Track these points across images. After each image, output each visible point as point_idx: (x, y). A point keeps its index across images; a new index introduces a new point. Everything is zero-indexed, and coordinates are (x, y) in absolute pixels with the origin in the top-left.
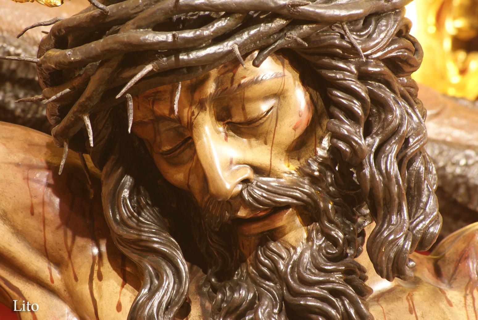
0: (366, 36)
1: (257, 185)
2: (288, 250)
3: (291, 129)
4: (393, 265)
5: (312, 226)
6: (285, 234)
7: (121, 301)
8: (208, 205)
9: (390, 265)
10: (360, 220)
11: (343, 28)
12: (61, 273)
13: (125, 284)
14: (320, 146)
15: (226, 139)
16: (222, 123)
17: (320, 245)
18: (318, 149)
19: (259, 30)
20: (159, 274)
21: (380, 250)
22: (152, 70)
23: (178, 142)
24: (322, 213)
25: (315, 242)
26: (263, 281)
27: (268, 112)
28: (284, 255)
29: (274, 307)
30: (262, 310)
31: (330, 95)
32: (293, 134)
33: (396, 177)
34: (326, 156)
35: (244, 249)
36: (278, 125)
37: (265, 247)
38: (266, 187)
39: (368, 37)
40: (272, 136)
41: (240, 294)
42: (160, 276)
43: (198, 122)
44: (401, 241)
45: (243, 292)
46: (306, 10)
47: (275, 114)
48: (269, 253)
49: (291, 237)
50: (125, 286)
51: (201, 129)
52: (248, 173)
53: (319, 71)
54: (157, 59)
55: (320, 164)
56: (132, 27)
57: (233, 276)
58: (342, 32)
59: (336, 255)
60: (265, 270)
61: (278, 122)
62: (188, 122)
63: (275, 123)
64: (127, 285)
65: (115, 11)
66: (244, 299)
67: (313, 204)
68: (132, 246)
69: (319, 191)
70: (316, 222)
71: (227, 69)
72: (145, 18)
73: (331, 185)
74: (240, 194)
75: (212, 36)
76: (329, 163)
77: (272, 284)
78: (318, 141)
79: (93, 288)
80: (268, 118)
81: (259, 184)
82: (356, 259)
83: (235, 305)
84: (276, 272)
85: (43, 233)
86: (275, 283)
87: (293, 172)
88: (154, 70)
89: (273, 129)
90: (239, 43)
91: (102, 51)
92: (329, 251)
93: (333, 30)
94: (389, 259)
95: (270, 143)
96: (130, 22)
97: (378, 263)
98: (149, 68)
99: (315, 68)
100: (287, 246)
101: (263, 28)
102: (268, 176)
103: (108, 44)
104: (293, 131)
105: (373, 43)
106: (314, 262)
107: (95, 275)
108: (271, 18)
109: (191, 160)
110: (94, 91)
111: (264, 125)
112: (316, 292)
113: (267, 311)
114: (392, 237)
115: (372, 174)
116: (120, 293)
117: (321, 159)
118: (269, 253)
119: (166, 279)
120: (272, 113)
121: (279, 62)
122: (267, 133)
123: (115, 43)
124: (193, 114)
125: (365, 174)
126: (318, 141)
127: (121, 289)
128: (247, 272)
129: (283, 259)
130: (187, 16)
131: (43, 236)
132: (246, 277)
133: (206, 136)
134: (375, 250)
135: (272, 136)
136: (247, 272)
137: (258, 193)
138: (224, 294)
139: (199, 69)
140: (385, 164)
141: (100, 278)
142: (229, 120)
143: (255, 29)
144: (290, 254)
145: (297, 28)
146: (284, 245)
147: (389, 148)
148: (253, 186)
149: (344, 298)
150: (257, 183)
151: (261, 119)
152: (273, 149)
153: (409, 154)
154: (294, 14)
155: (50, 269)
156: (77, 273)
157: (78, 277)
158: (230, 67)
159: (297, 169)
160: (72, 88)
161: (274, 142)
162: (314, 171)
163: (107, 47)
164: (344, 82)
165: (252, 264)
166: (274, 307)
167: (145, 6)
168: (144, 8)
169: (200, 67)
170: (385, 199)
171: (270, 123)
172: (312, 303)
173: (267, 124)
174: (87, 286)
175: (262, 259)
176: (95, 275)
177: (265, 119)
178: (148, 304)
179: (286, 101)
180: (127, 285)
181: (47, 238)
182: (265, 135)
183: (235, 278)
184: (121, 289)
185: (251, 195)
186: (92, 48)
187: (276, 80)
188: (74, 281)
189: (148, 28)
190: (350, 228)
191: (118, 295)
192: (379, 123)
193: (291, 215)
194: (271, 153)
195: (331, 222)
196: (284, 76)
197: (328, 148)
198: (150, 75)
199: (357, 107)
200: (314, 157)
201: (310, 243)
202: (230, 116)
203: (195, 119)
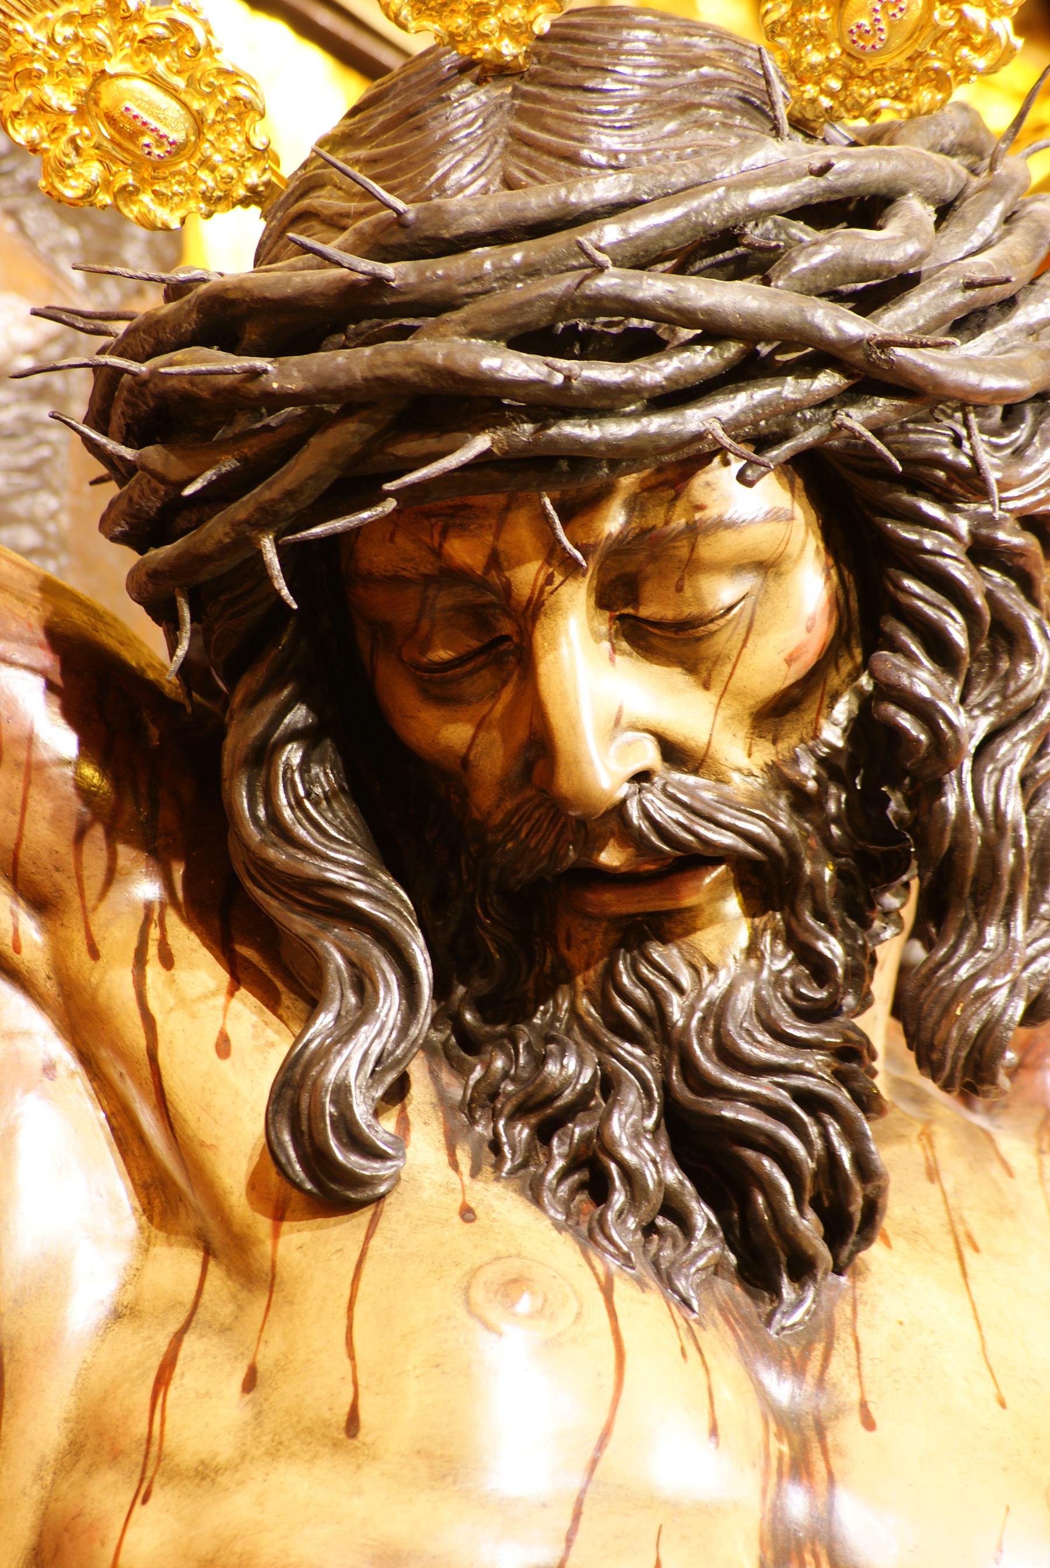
0: (1009, 451)
1: (664, 791)
2: (696, 970)
3: (779, 660)
4: (969, 1054)
5: (765, 918)
6: (694, 930)
7: (230, 1032)
8: (513, 822)
9: (963, 1054)
10: (877, 924)
11: (966, 424)
12: (44, 928)
13: (237, 989)
14: (828, 717)
15: (612, 660)
16: (608, 614)
17: (781, 972)
18: (823, 722)
19: (780, 393)
20: (367, 981)
21: (947, 1009)
22: (488, 452)
23: (475, 644)
24: (803, 889)
25: (767, 962)
26: (616, 1040)
27: (730, 609)
28: (685, 979)
29: (646, 1113)
30: (623, 1117)
31: (891, 588)
32: (783, 673)
33: (1016, 829)
34: (840, 744)
35: (569, 947)
36: (749, 645)
37: (635, 952)
38: (685, 798)
39: (1013, 453)
40: (728, 669)
41: (562, 1066)
42: (369, 987)
43: (557, 602)
44: (999, 998)
45: (571, 1063)
46: (909, 360)
47: (747, 614)
48: (645, 970)
49: (706, 940)
50: (237, 993)
51: (561, 622)
52: (649, 756)
53: (878, 519)
54: (506, 424)
55: (821, 761)
56: (462, 329)
57: (534, 1015)
58: (964, 432)
59: (819, 1005)
60: (628, 1011)
61: (752, 637)
62: (530, 600)
63: (742, 637)
64: (243, 992)
65: (412, 279)
66: (567, 1083)
67: (786, 863)
68: (293, 893)
69: (806, 830)
70: (775, 910)
71: (661, 478)
72: (497, 313)
73: (837, 820)
74: (620, 808)
75: (662, 387)
76: (842, 763)
77: (639, 1052)
78: (827, 701)
79: (144, 984)
80: (730, 621)
81: (670, 790)
82: (855, 1021)
83: (547, 1091)
84: (657, 1023)
85: (18, 818)
86: (648, 1052)
87: (757, 772)
88: (495, 450)
89: (735, 653)
90: (724, 418)
91: (365, 380)
92: (803, 990)
93: (938, 421)
94: (964, 1036)
95: (717, 687)
96: (455, 316)
97: (936, 1042)
98: (482, 443)
99: (867, 512)
100: (695, 961)
101: (791, 388)
102: (695, 772)
103: (386, 364)
104: (784, 666)
105: (1028, 470)
106: (764, 1015)
107: (153, 951)
108: (808, 367)
109: (493, 696)
110: (310, 477)
111: (716, 639)
112: (764, 1091)
113: (631, 1121)
114: (981, 984)
115: (962, 811)
116: (225, 1009)
117: (826, 750)
118: (645, 970)
119: (386, 994)
120: (742, 609)
121: (785, 480)
122: (718, 660)
123: (408, 364)
124: (549, 580)
125: (944, 809)
126: (827, 701)
127: (228, 1001)
128: (573, 1010)
129: (680, 990)
130: (593, 324)
131: (16, 825)
132: (567, 1024)
133: (570, 644)
134: (931, 1010)
135: (728, 669)
136: (573, 1010)
137: (667, 814)
138: (513, 1059)
139: (601, 468)
140: (993, 789)
141: (167, 960)
142: (629, 610)
143: (771, 386)
144: (700, 981)
145: (865, 400)
146: (689, 957)
147: (1009, 750)
148: (655, 791)
149: (827, 1118)
150: (665, 785)
151: (712, 621)
152: (723, 704)
153: (1043, 772)
154: (879, 367)
155: (13, 914)
156: (97, 939)
157: (99, 948)
158: (670, 475)
159: (767, 765)
160: (243, 459)
161: (730, 686)
162: (806, 777)
163: (383, 372)
164: (939, 560)
165: (588, 993)
166: (646, 1113)
167: (497, 280)
168: (495, 285)
169: (604, 463)
170: (976, 880)
171: (732, 634)
172: (749, 1117)
173: (722, 637)
174: (129, 978)
175: (625, 980)
176: (153, 951)
177: (722, 622)
178: (339, 1052)
179: (780, 586)
180: (243, 992)
181: (26, 832)
182: (709, 664)
183: (537, 1021)
184: (228, 1001)
185: (647, 815)
186: (338, 367)
187: (773, 526)
188: (86, 957)
189: (498, 340)
190: (856, 940)
191: (220, 1014)
192: (989, 680)
193: (719, 881)
194: (716, 713)
195: (820, 915)
196: (792, 519)
197: (845, 723)
198: (484, 460)
199: (957, 631)
200: (811, 743)
201: (753, 963)
202: (634, 600)
203: (552, 593)
